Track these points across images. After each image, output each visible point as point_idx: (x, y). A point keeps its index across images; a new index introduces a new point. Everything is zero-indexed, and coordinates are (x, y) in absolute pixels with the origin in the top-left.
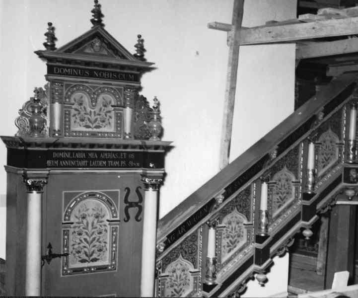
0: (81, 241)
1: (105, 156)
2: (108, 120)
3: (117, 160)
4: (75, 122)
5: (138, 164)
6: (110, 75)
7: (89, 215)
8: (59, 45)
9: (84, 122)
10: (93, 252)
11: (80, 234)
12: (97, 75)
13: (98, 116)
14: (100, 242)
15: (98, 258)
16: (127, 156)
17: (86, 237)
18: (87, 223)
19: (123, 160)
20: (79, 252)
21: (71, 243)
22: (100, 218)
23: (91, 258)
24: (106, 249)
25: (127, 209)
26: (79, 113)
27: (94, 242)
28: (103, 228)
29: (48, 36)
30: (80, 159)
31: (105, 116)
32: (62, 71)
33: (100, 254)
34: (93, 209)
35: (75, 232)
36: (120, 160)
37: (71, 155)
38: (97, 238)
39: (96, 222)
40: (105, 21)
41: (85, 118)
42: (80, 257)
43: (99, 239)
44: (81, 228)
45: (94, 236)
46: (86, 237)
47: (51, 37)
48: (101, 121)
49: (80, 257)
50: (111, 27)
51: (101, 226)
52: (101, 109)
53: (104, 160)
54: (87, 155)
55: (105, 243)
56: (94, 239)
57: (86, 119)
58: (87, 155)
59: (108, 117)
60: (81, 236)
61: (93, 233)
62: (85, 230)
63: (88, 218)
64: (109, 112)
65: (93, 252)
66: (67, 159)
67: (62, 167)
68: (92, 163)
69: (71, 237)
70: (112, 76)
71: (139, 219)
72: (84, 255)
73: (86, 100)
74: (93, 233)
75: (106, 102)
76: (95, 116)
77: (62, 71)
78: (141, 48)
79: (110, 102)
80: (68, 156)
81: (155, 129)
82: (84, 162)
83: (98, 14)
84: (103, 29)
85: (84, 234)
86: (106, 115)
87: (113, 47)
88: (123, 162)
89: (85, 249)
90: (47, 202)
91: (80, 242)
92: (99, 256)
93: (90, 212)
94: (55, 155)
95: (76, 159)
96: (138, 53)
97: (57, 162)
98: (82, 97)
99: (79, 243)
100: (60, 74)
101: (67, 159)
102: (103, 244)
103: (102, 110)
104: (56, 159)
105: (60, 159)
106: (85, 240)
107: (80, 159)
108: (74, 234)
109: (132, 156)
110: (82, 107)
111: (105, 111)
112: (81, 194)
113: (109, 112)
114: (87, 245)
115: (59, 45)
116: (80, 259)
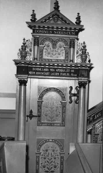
0: (45, 162)
1: (59, 71)
2: (62, 54)
3: (65, 73)
4: (45, 55)
5: (76, 75)
6: (62, 33)
7: (49, 150)
8: (38, 17)
9: (50, 55)
10: (52, 168)
11: (45, 159)
12: (56, 33)
13: (57, 52)
14: (55, 163)
15: (56, 119)
16: (70, 71)
17: (48, 160)
18: (49, 154)
19: (68, 73)
20: (44, 167)
21: (40, 163)
22: (55, 151)
23: (51, 170)
24: (58, 167)
25: (71, 98)
26: (47, 51)
27: (52, 163)
28: (57, 157)
29: (32, 16)
30: (46, 72)
31: (60, 52)
32: (39, 31)
33: (55, 169)
34: (52, 147)
35: (42, 157)
36: (66, 73)
37: (42, 69)
38: (54, 161)
39: (53, 153)
40: (60, 9)
41: (50, 53)
42: (45, 170)
43: (54, 162)
44: (45, 156)
45: (52, 160)
46: (48, 160)
47: (34, 15)
48: (54, 158)
49: (45, 170)
50: (64, 11)
51: (55, 155)
52: (58, 49)
53: (58, 72)
54: (49, 70)
55: (58, 164)
56: (52, 161)
57: (51, 53)
58: (49, 70)
59: (62, 53)
60: (45, 160)
61: (52, 159)
62: (48, 157)
63: (49, 151)
64: (63, 50)
65: (52, 168)
66: (39, 71)
67: (37, 75)
68: (52, 74)
69: (40, 159)
70: (64, 33)
71: (77, 102)
72: (47, 169)
73: (51, 45)
74: (52, 159)
75: (61, 45)
76: (55, 52)
77: (39, 31)
78: (78, 18)
79: (63, 46)
80: (40, 70)
81: (84, 56)
82: (47, 73)
83: (57, 7)
84: (60, 13)
85: (47, 158)
86: (61, 52)
87: (65, 20)
88: (68, 74)
89: (50, 115)
90: (29, 132)
91: (45, 162)
92: (54, 170)
93: (50, 148)
94: (34, 69)
95: (44, 71)
96: (77, 21)
97: (34, 73)
98: (49, 43)
99: (45, 163)
100: (37, 33)
101: (39, 71)
102: (57, 164)
103: (59, 49)
104: (34, 71)
105: (36, 71)
106: (48, 161)
107: (46, 72)
108: (42, 158)
109: (73, 71)
110: (49, 48)
111: (60, 50)
112: (45, 140)
113: (63, 50)
114: (48, 164)
115: (38, 17)
116: (45, 171)
